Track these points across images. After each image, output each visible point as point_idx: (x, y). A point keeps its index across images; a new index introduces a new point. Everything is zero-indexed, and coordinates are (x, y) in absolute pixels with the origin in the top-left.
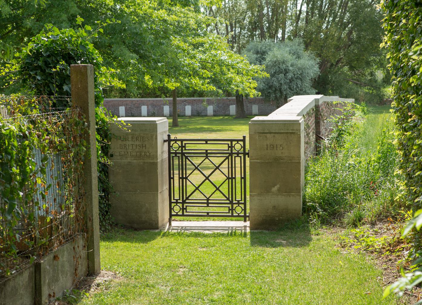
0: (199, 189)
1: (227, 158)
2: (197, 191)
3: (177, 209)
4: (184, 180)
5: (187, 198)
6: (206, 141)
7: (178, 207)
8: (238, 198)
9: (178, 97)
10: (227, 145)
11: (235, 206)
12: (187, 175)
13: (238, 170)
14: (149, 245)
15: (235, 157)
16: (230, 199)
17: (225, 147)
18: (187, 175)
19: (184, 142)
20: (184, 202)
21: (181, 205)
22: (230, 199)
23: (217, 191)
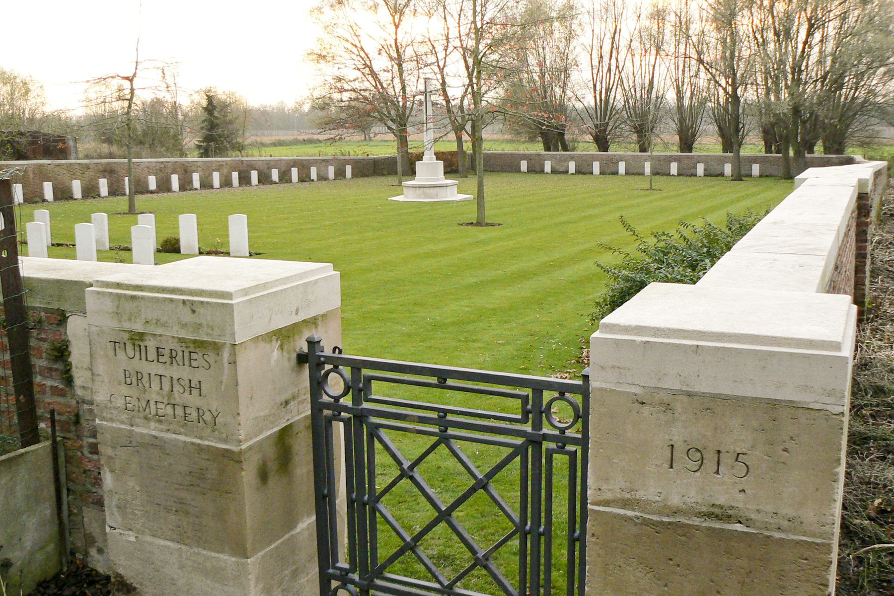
4: (435, 429)
19: (365, 372)
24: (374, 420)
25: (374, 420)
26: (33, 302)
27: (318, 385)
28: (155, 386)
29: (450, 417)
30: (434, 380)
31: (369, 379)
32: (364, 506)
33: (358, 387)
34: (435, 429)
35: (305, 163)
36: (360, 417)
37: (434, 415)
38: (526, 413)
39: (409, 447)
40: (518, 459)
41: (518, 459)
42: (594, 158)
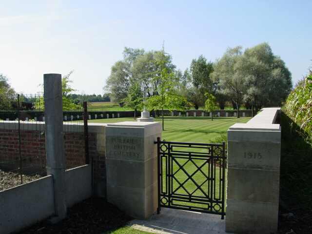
0: (199, 190)
1: (207, 197)
2: (184, 167)
3: (217, 208)
4: (188, 157)
5: (207, 197)
6: (223, 180)
7: (218, 206)
8: (174, 202)
9: (65, 121)
10: (219, 198)
11: (167, 152)
12: (193, 160)
13: (196, 205)
14: (284, 61)
15: (172, 151)
16: (171, 158)
17: (217, 196)
18: (193, 160)
19: (171, 145)
20: (211, 200)
21: (213, 204)
22: (171, 158)
23: (184, 185)
24: (173, 156)
25: (173, 156)
26: (89, 131)
27: (159, 148)
28: (123, 148)
29: (192, 154)
30: (188, 146)
31: (172, 146)
32: (170, 176)
33: (169, 148)
34: (188, 157)
35: (212, 69)
36: (170, 155)
37: (188, 154)
38: (209, 151)
39: (181, 161)
40: (173, 191)
41: (173, 191)
42: (194, 111)
